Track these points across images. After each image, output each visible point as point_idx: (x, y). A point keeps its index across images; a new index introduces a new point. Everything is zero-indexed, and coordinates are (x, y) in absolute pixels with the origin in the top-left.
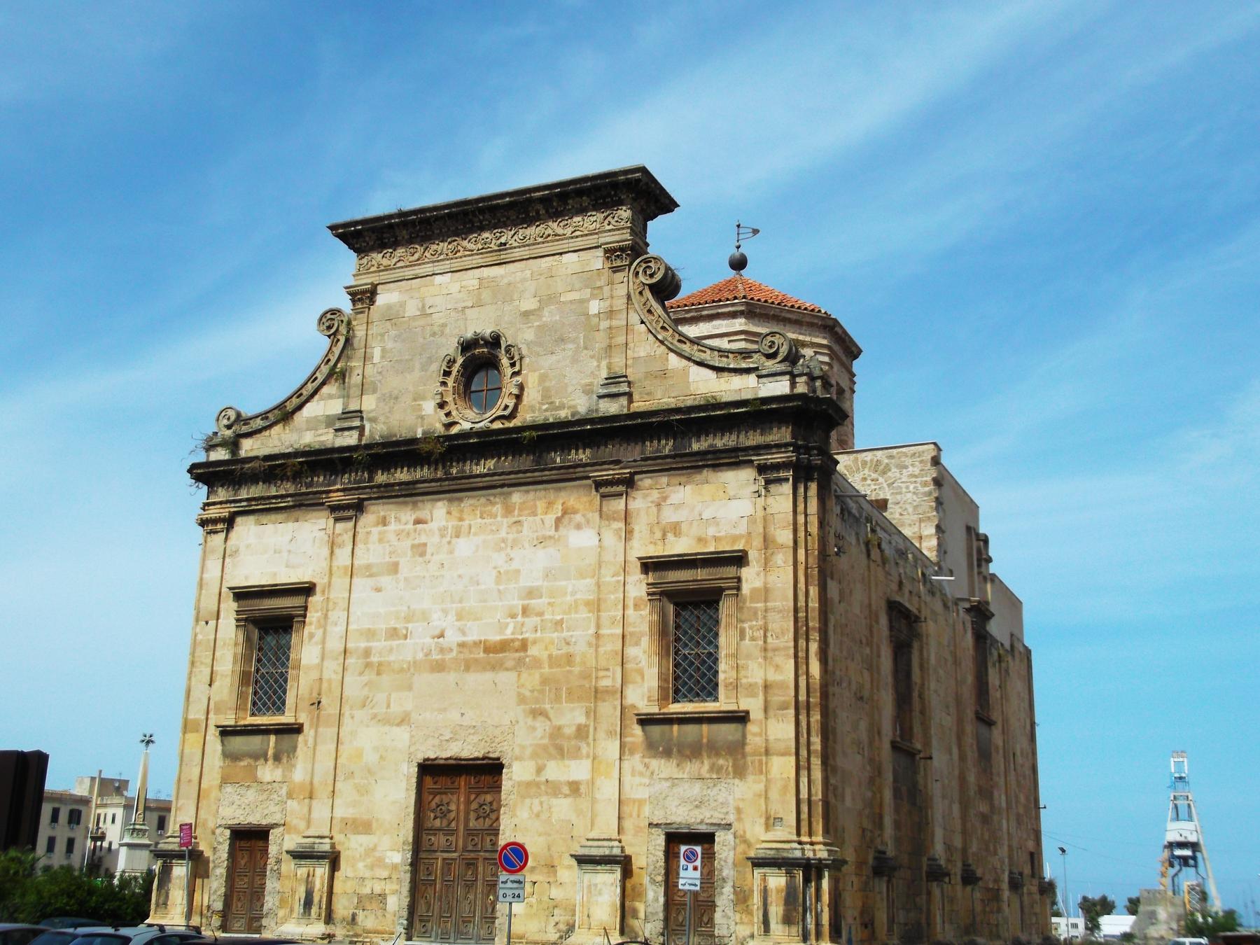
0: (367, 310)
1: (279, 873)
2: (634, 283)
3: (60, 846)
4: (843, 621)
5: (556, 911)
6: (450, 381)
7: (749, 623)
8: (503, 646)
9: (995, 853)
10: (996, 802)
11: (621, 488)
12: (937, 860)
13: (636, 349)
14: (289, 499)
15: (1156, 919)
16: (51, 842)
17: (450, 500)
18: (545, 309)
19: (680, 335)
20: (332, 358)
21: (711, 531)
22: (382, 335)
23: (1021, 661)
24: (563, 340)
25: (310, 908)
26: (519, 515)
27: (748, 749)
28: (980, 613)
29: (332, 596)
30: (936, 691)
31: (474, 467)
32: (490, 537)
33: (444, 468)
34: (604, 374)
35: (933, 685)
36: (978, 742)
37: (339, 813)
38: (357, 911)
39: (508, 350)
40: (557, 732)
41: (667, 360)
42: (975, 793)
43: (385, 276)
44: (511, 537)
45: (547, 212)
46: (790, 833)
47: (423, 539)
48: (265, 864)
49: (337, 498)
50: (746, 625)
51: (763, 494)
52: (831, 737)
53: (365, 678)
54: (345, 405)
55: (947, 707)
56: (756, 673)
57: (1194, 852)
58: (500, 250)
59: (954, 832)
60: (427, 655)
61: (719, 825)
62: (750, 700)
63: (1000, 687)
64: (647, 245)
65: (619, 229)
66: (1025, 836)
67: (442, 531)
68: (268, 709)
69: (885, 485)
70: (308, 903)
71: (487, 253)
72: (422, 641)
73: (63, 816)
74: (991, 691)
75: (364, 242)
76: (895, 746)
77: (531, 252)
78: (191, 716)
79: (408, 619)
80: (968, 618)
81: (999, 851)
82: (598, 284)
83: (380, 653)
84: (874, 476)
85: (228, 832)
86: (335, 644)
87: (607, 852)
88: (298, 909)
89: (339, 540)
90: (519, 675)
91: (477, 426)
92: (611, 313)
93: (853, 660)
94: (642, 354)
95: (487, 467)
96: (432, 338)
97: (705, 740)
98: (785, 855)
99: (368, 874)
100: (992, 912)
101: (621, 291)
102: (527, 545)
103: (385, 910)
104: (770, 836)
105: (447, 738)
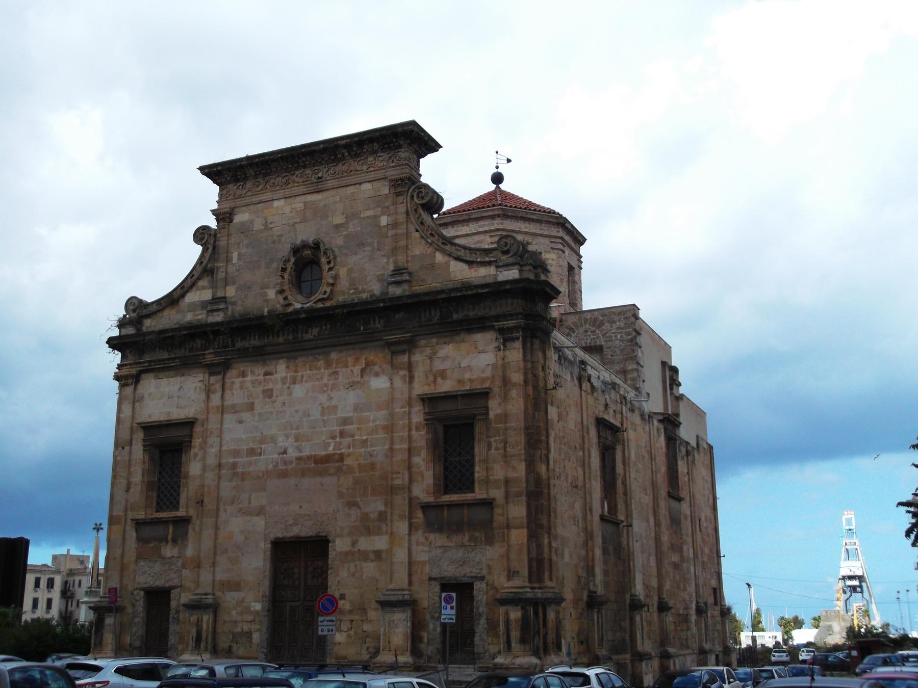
0: (227, 226)
1: (178, 620)
2: (411, 203)
3: (42, 605)
4: (561, 434)
5: (368, 640)
6: (286, 276)
7: (494, 438)
8: (327, 459)
9: (685, 589)
10: (685, 554)
11: (405, 347)
12: (637, 596)
13: (413, 249)
14: (177, 360)
15: (833, 631)
16: (35, 602)
17: (288, 358)
18: (350, 223)
19: (443, 239)
20: (203, 260)
21: (467, 376)
22: (238, 244)
23: (705, 454)
24: (363, 244)
25: (200, 643)
26: (336, 368)
27: (495, 524)
28: (670, 422)
29: (209, 428)
30: (636, 479)
31: (304, 335)
32: (317, 383)
33: (283, 335)
34: (391, 267)
35: (633, 475)
36: (670, 513)
37: (219, 577)
38: (232, 644)
39: (325, 253)
40: (365, 517)
41: (435, 256)
42: (668, 548)
43: (239, 202)
44: (331, 382)
45: (349, 154)
46: (524, 581)
47: (270, 386)
48: (169, 614)
49: (210, 358)
50: (492, 440)
51: (502, 348)
52: (552, 514)
53: (234, 484)
54: (214, 294)
55: (645, 490)
56: (499, 473)
57: (860, 582)
58: (318, 182)
59: (651, 576)
60: (275, 466)
61: (476, 577)
62: (495, 491)
63: (688, 473)
64: (420, 175)
65: (399, 166)
66: (709, 577)
67: (284, 380)
68: (168, 507)
69: (600, 335)
70: (198, 640)
71: (309, 184)
72: (271, 457)
73: (43, 583)
74: (680, 477)
75: (223, 178)
76: (602, 518)
77: (340, 183)
78: (115, 514)
79: (263, 441)
80: (661, 426)
81: (688, 588)
82: (387, 204)
83: (243, 466)
84: (593, 329)
85: (142, 593)
86: (211, 461)
87: (401, 598)
88: (192, 644)
89: (213, 388)
90: (339, 479)
91: (305, 306)
92: (395, 225)
93: (569, 460)
94: (417, 253)
95: (313, 334)
96: (273, 245)
97: (466, 519)
98: (521, 596)
99: (239, 618)
100: (682, 630)
101: (402, 209)
102: (341, 387)
103: (251, 642)
104: (510, 584)
105: (290, 523)
